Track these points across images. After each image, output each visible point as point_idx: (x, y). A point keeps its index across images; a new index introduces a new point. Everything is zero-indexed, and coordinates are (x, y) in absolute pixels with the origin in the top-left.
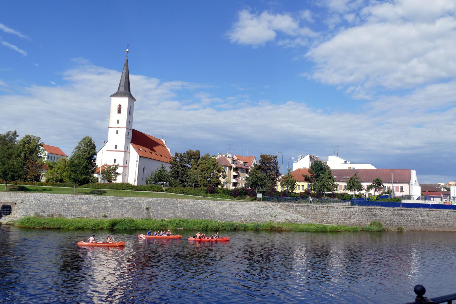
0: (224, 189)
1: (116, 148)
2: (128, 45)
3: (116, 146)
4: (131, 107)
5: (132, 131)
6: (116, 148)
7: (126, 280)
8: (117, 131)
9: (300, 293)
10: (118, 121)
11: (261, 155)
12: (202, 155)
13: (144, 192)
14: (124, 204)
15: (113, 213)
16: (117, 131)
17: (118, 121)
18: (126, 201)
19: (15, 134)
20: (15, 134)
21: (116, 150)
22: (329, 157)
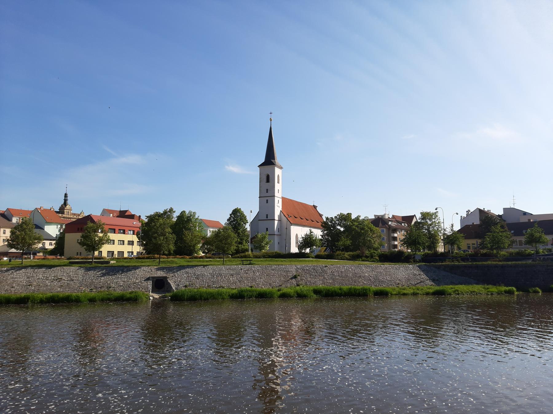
0: (97, 250)
1: (267, 217)
2: (271, 113)
3: (267, 215)
4: (278, 175)
5: (281, 199)
6: (267, 217)
7: (320, 334)
8: (267, 200)
9: (459, 408)
10: (267, 190)
11: (422, 212)
12: (353, 217)
13: (305, 260)
14: (272, 273)
15: (261, 282)
16: (267, 200)
17: (267, 190)
18: (273, 270)
19: (171, 210)
20: (171, 210)
21: (267, 219)
22: (528, 221)
